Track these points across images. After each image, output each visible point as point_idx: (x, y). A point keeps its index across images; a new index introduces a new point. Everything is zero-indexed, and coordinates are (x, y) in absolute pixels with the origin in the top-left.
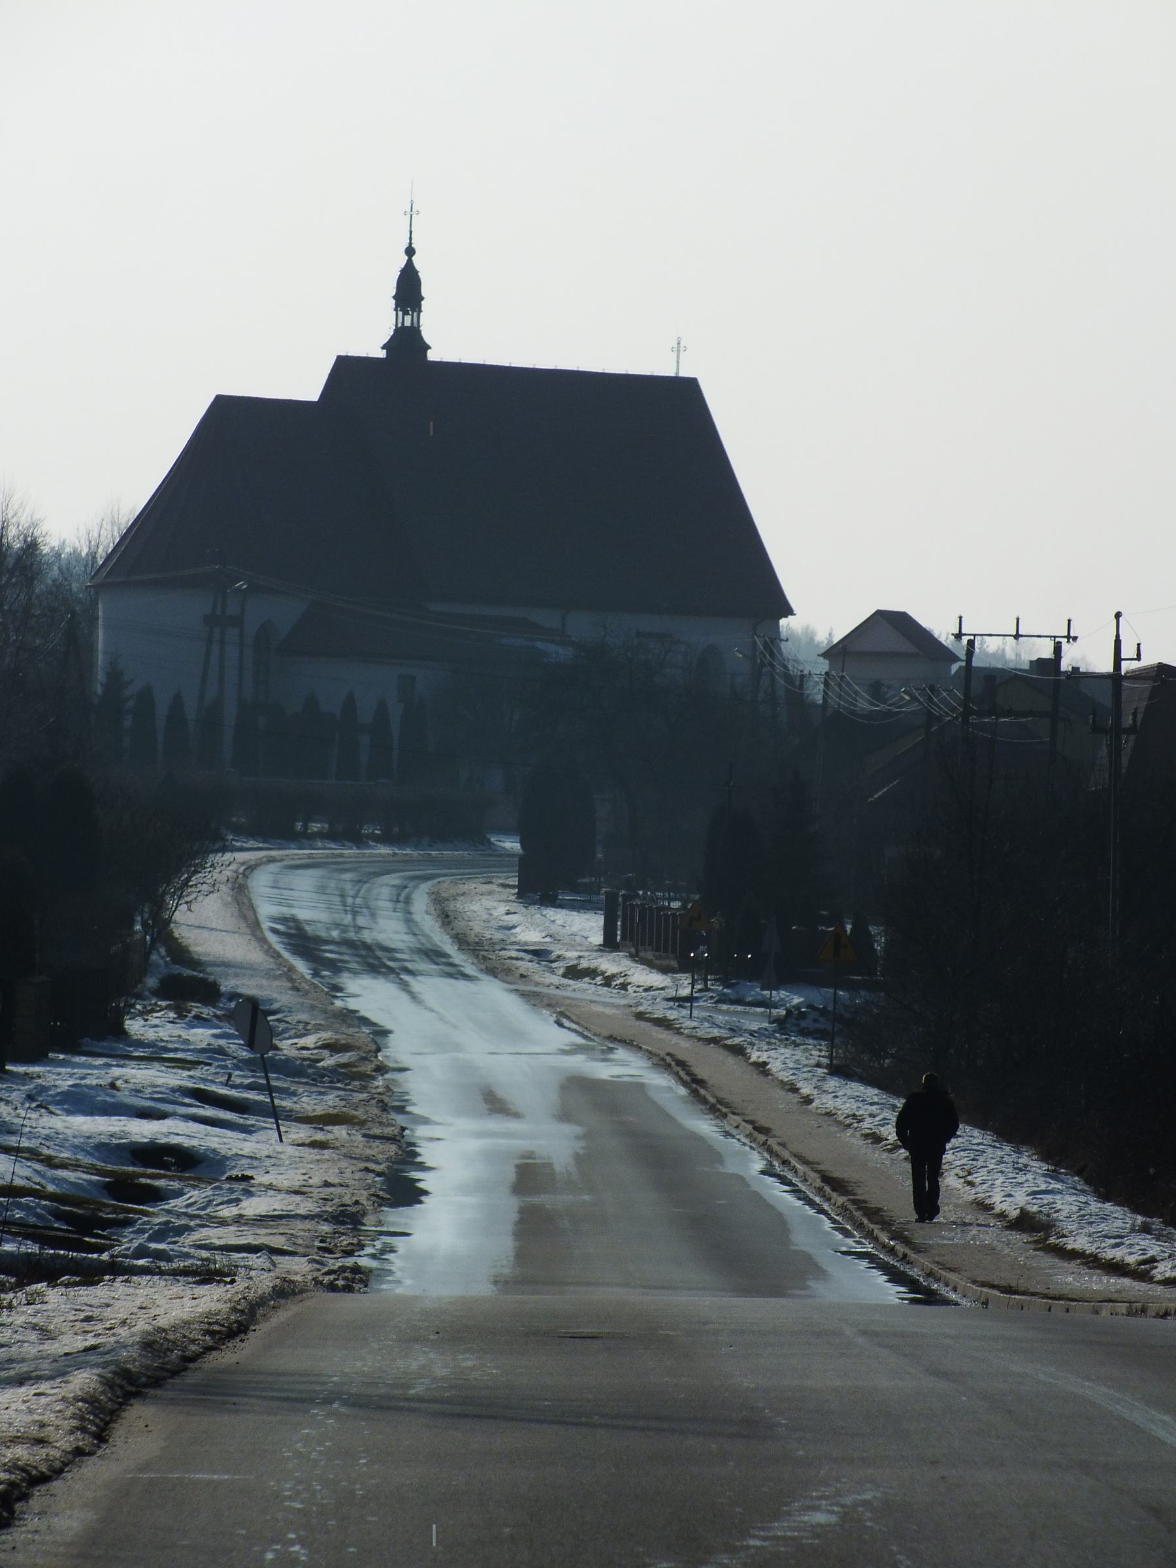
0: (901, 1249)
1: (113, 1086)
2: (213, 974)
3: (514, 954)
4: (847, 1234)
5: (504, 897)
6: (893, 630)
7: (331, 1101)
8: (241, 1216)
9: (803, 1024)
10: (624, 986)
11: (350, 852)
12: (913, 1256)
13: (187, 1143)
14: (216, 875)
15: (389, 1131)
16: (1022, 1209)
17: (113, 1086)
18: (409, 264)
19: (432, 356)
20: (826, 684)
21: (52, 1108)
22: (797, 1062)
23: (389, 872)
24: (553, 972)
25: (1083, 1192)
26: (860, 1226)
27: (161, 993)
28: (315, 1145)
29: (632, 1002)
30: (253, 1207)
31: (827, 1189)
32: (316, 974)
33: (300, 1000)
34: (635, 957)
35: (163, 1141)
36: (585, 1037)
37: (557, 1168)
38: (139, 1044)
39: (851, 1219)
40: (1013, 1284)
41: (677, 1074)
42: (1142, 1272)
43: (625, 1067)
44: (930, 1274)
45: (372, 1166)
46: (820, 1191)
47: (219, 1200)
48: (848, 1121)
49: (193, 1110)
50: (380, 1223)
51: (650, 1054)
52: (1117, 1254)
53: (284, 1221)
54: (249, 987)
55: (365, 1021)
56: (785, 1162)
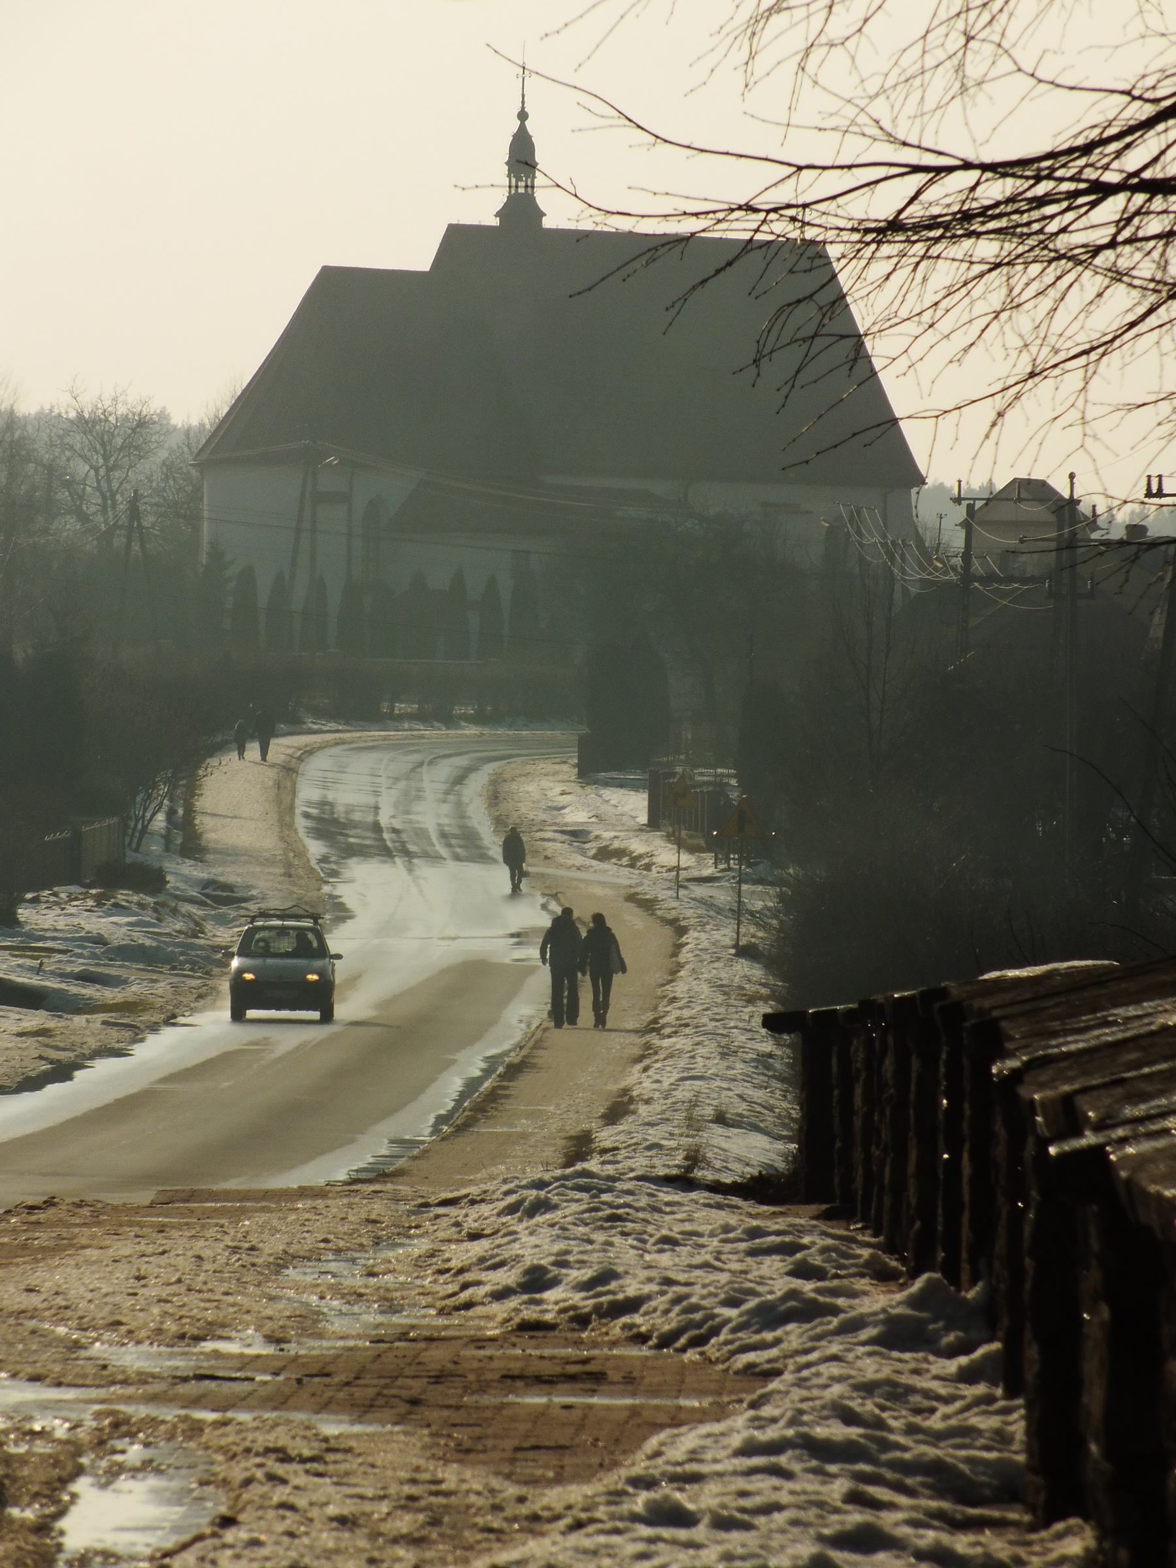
10: (648, 867)
19: (548, 223)
24: (583, 853)
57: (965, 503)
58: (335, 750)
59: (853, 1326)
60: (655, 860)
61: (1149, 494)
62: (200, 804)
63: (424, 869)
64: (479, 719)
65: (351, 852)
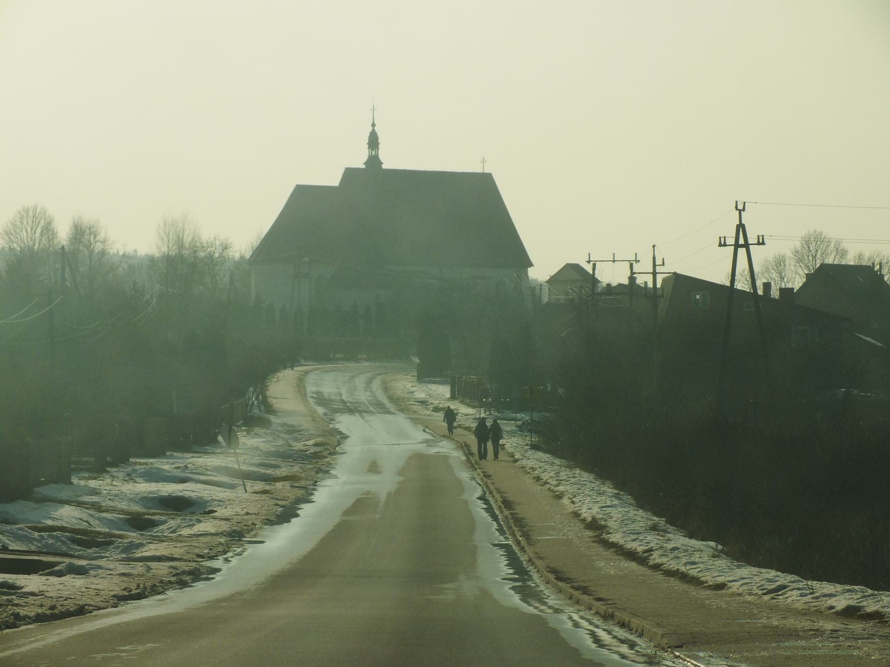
0: (523, 543)
1: (186, 466)
17: (186, 466)
18: (373, 131)
19: (384, 167)
24: (428, 409)
34: (462, 402)
35: (180, 494)
47: (184, 525)
58: (316, 372)
59: (118, 547)
61: (720, 245)
62: (268, 393)
63: (368, 417)
64: (367, 360)
65: (336, 411)
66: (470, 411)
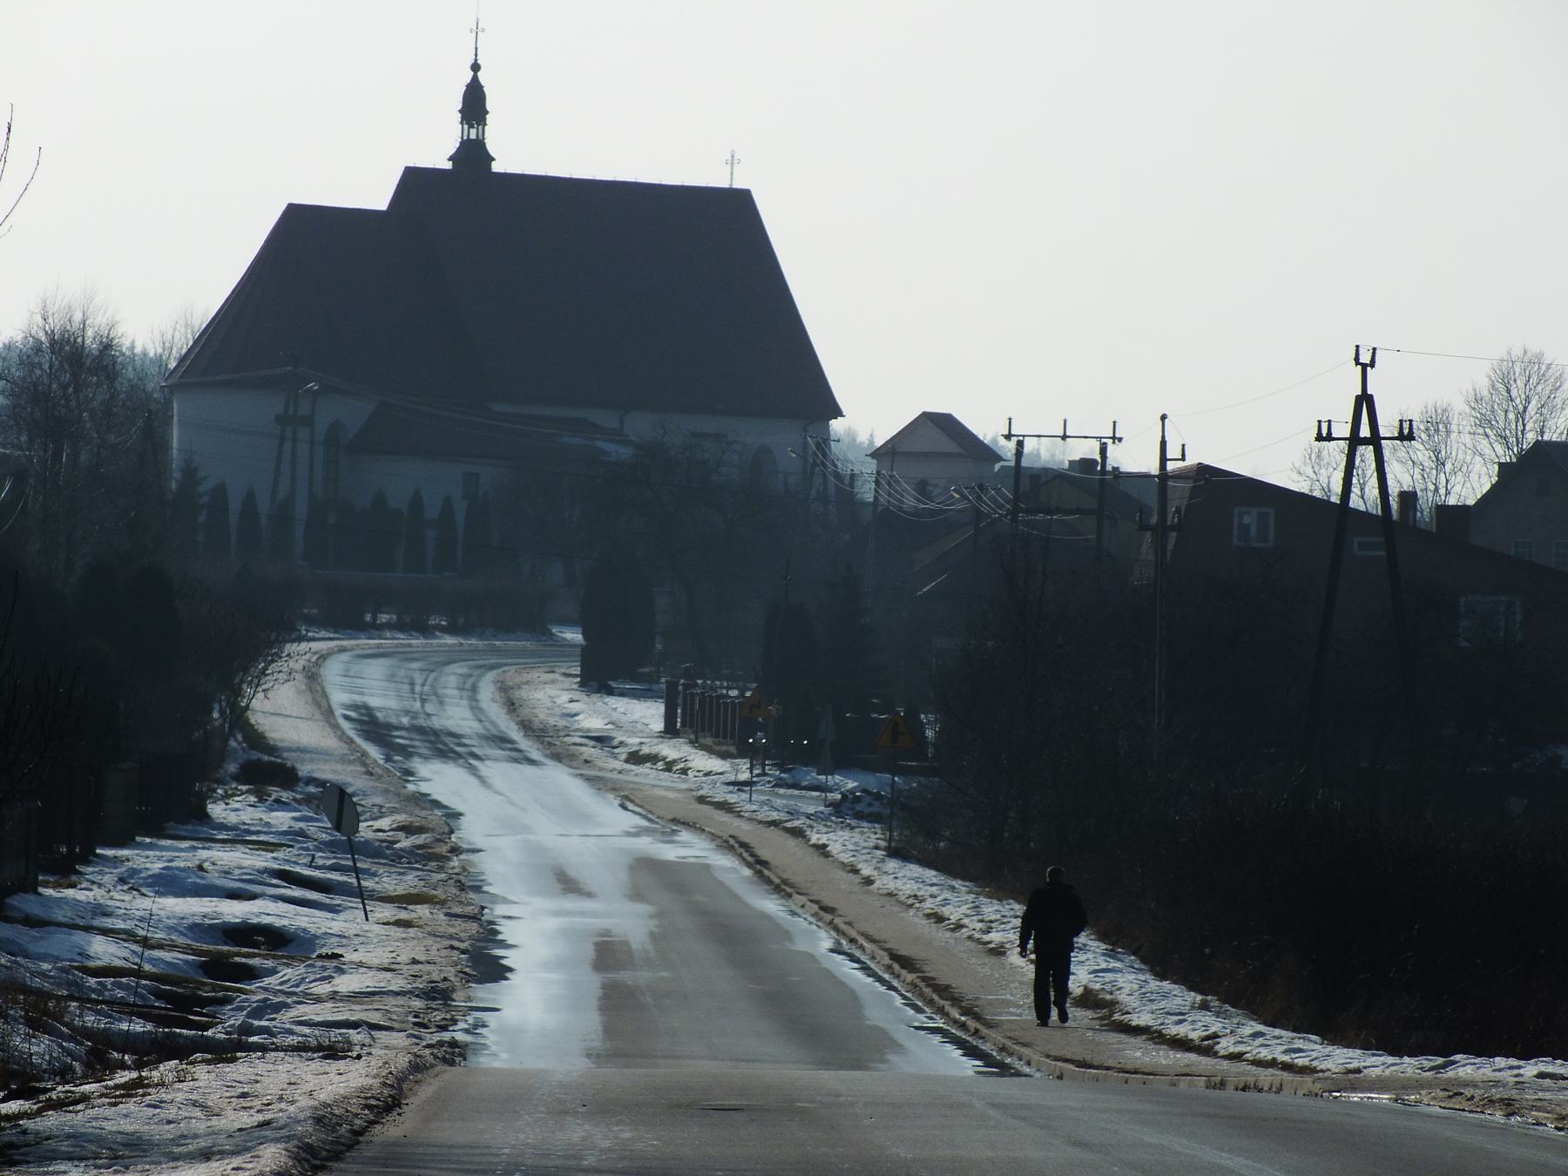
0: (972, 1024)
1: (200, 868)
2: (290, 759)
3: (578, 740)
4: (919, 1010)
5: (567, 686)
6: (939, 434)
7: (410, 882)
8: (335, 992)
9: (858, 807)
10: (684, 771)
11: (418, 642)
12: (984, 1031)
13: (278, 922)
14: (292, 664)
15: (469, 910)
16: (1086, 988)
17: (200, 868)
18: (475, 79)
19: (496, 167)
20: (877, 482)
21: (144, 890)
22: (856, 844)
23: (455, 662)
24: (615, 757)
25: (1140, 970)
26: (930, 1002)
27: (240, 777)
28: (398, 923)
29: (693, 786)
30: (347, 983)
31: (896, 966)
32: (388, 759)
33: (372, 784)
36: (650, 820)
37: (634, 946)
38: (223, 827)
39: (922, 995)
40: (1088, 1058)
41: (740, 855)
42: (1205, 1048)
43: (689, 849)
44: (1003, 1049)
45: (456, 944)
46: (889, 968)
48: (911, 901)
49: (282, 891)
50: (469, 999)
51: (713, 837)
52: (1181, 1030)
53: (377, 998)
54: (327, 771)
55: (436, 804)
56: (852, 941)
57: (1014, 439)
59: (241, 1009)
60: (690, 765)
61: (1319, 438)
64: (452, 630)
66: (716, 764)
